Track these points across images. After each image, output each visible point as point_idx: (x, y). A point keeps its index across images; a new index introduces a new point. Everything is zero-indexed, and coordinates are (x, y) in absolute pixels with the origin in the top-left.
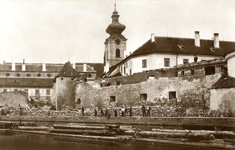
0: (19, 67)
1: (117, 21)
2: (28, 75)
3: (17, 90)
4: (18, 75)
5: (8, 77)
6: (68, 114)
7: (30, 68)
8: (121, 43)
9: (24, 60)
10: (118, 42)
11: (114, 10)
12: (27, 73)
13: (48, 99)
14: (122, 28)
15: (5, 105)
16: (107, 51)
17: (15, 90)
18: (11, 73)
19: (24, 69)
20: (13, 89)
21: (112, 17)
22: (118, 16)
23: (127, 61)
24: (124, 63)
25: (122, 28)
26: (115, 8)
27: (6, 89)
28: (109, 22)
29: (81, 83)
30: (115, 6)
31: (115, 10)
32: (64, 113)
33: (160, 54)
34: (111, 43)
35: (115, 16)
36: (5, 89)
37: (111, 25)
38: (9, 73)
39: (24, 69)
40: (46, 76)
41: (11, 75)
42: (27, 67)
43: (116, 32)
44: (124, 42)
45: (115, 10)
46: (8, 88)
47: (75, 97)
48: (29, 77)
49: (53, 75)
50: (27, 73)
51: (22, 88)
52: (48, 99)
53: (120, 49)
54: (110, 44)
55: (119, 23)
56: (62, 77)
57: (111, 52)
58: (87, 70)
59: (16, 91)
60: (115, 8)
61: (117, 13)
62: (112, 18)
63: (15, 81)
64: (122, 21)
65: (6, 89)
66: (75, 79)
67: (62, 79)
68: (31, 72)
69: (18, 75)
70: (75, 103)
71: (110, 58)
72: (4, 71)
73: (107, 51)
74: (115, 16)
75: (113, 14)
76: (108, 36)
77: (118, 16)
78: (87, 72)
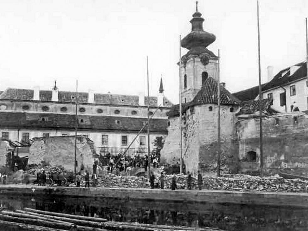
0: (46, 96)
1: (200, 27)
2: (64, 109)
3: (48, 134)
4: (45, 108)
5: (27, 111)
6: (278, 186)
7: (66, 98)
8: (210, 63)
9: (55, 82)
10: (205, 61)
11: (195, 11)
12: (62, 105)
13: (104, 152)
14: (211, 39)
15: (42, 162)
16: (185, 76)
17: (44, 134)
18: (31, 103)
19: (55, 98)
20: (40, 134)
21: (191, 22)
22: (203, 20)
23: (295, 82)
24: (285, 86)
25: (211, 39)
26: (197, 7)
27: (8, 133)
28: (187, 30)
29: (255, 117)
30: (196, 4)
31: (197, 10)
32: (264, 184)
33: (302, 80)
34: (194, 61)
35: (197, 20)
36: (5, 133)
37: (191, 33)
38: (28, 103)
39: (55, 98)
40: (94, 112)
41: (32, 108)
42: (60, 95)
43: (198, 43)
44: (214, 61)
45: (197, 10)
46: (31, 131)
47: (238, 147)
48: (64, 113)
49: (106, 110)
50: (62, 105)
51: (58, 131)
52: (104, 152)
53: (208, 72)
54: (193, 65)
55: (205, 32)
56: (210, 105)
57: (195, 77)
58: (164, 104)
59: (46, 137)
60: (197, 7)
61: (199, 15)
62: (191, 24)
63: (43, 119)
64: (208, 28)
65: (28, 133)
66: (236, 110)
67: (211, 109)
68: (68, 103)
69: (45, 108)
70: (239, 160)
71: (193, 87)
72: (18, 100)
73: (185, 76)
74: (197, 20)
75: (193, 18)
76: (185, 51)
77: (203, 20)
78: (164, 107)
